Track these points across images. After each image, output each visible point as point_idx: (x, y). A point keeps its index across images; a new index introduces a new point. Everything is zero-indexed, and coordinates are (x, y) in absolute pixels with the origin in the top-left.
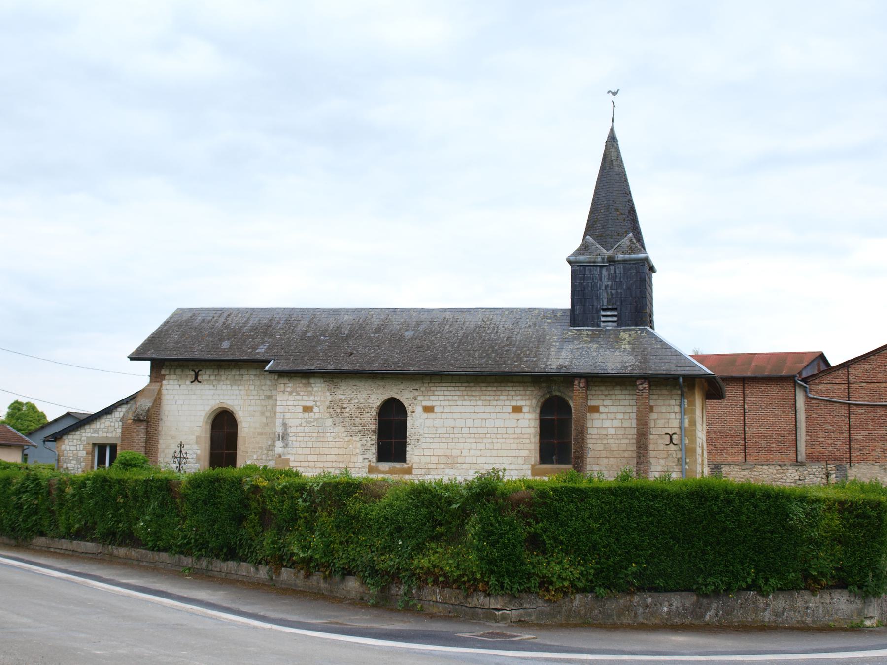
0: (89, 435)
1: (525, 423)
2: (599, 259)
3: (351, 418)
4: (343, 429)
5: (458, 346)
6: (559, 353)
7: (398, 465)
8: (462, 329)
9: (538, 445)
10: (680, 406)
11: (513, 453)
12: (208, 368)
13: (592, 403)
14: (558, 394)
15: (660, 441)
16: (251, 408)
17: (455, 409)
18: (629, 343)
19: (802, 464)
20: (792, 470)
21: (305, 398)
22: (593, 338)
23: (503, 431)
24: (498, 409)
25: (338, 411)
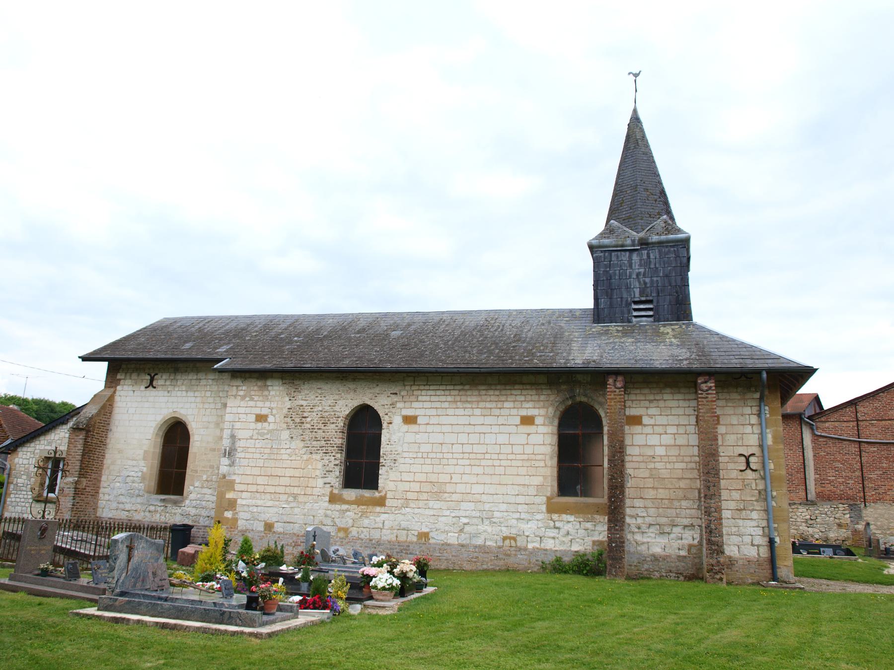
0: (42, 447)
1: (539, 439)
2: (629, 242)
3: (312, 430)
4: (302, 444)
5: (453, 344)
6: (583, 347)
7: (367, 493)
8: (460, 327)
9: (555, 470)
10: (759, 415)
11: (520, 480)
12: (165, 370)
13: (632, 412)
14: (584, 399)
15: (731, 466)
16: (205, 419)
17: (444, 420)
18: (675, 337)
19: (813, 503)
20: (802, 509)
21: (260, 404)
22: (625, 333)
23: (508, 449)
24: (501, 420)
25: (298, 420)
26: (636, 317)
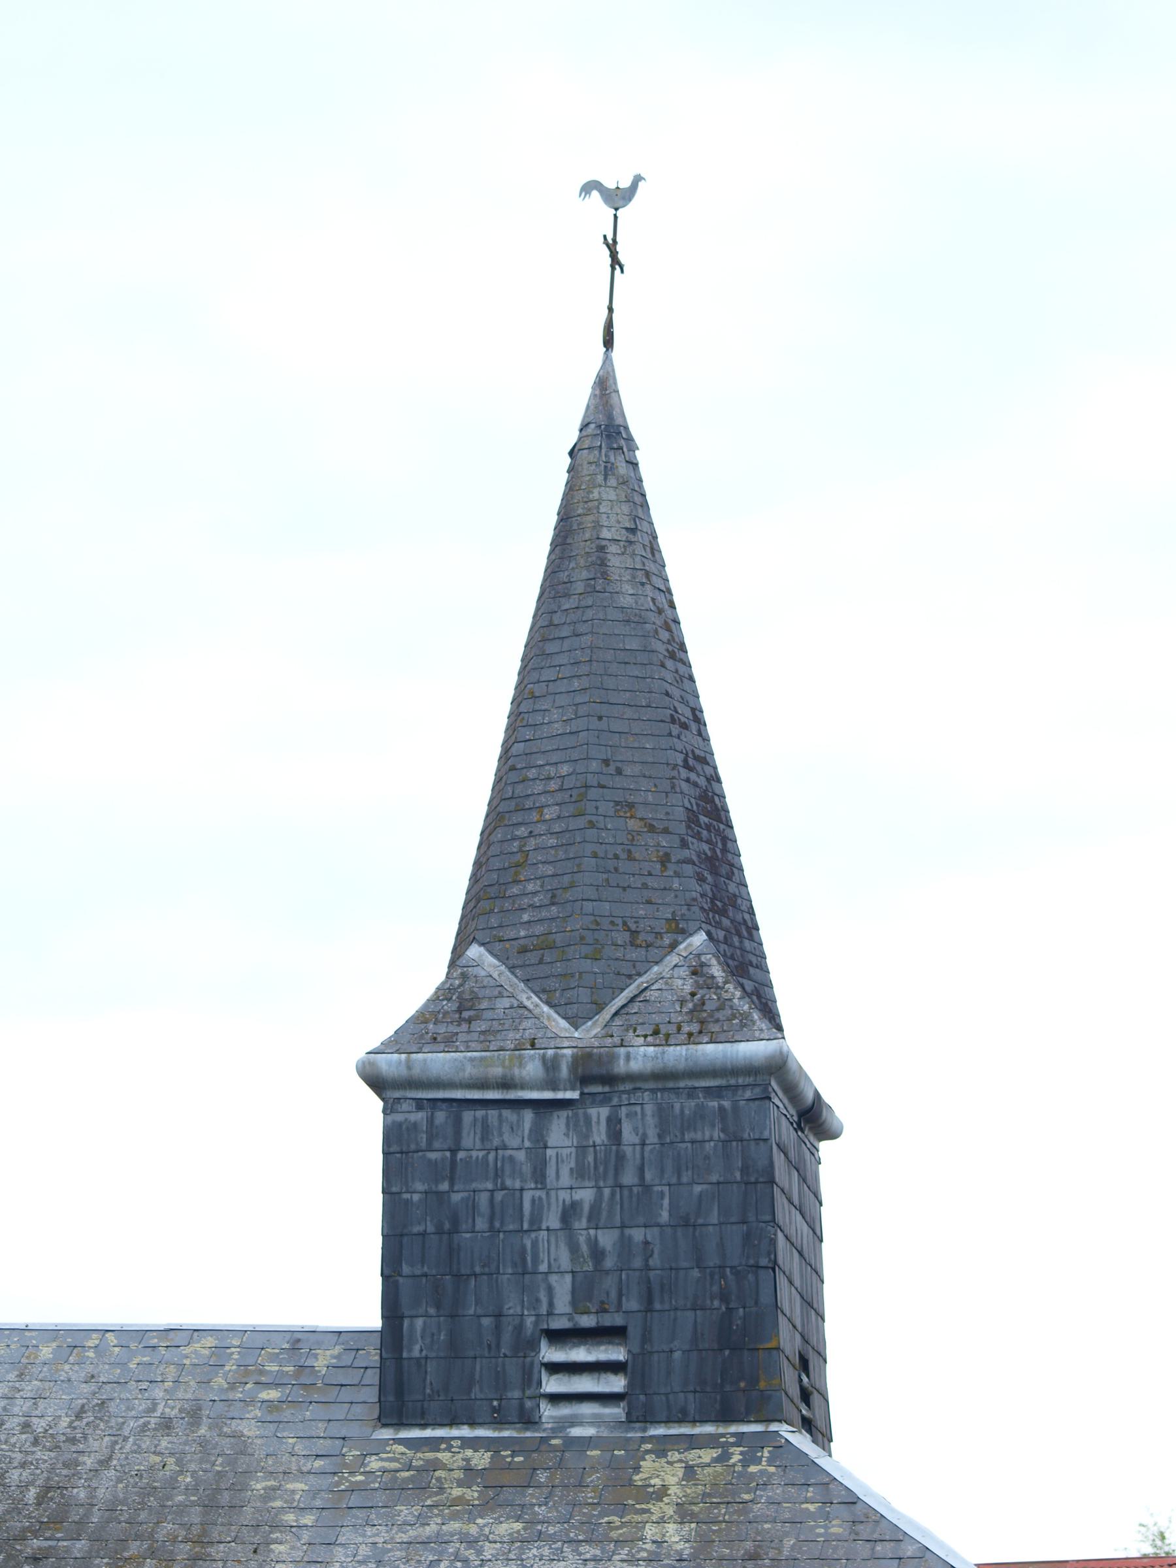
2: (532, 1068)
18: (684, 1514)
22: (498, 1488)
26: (555, 1398)
